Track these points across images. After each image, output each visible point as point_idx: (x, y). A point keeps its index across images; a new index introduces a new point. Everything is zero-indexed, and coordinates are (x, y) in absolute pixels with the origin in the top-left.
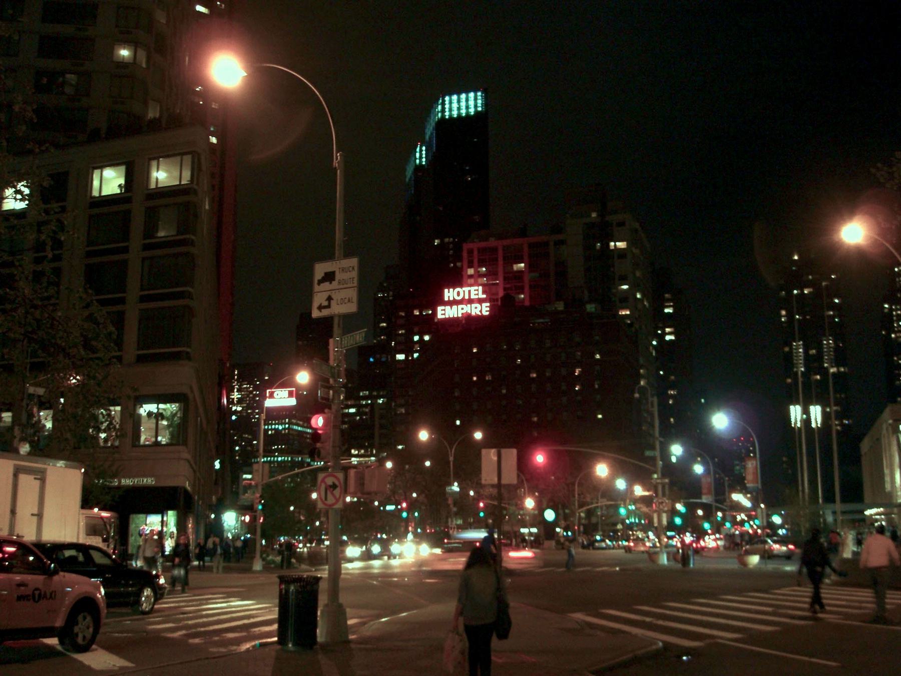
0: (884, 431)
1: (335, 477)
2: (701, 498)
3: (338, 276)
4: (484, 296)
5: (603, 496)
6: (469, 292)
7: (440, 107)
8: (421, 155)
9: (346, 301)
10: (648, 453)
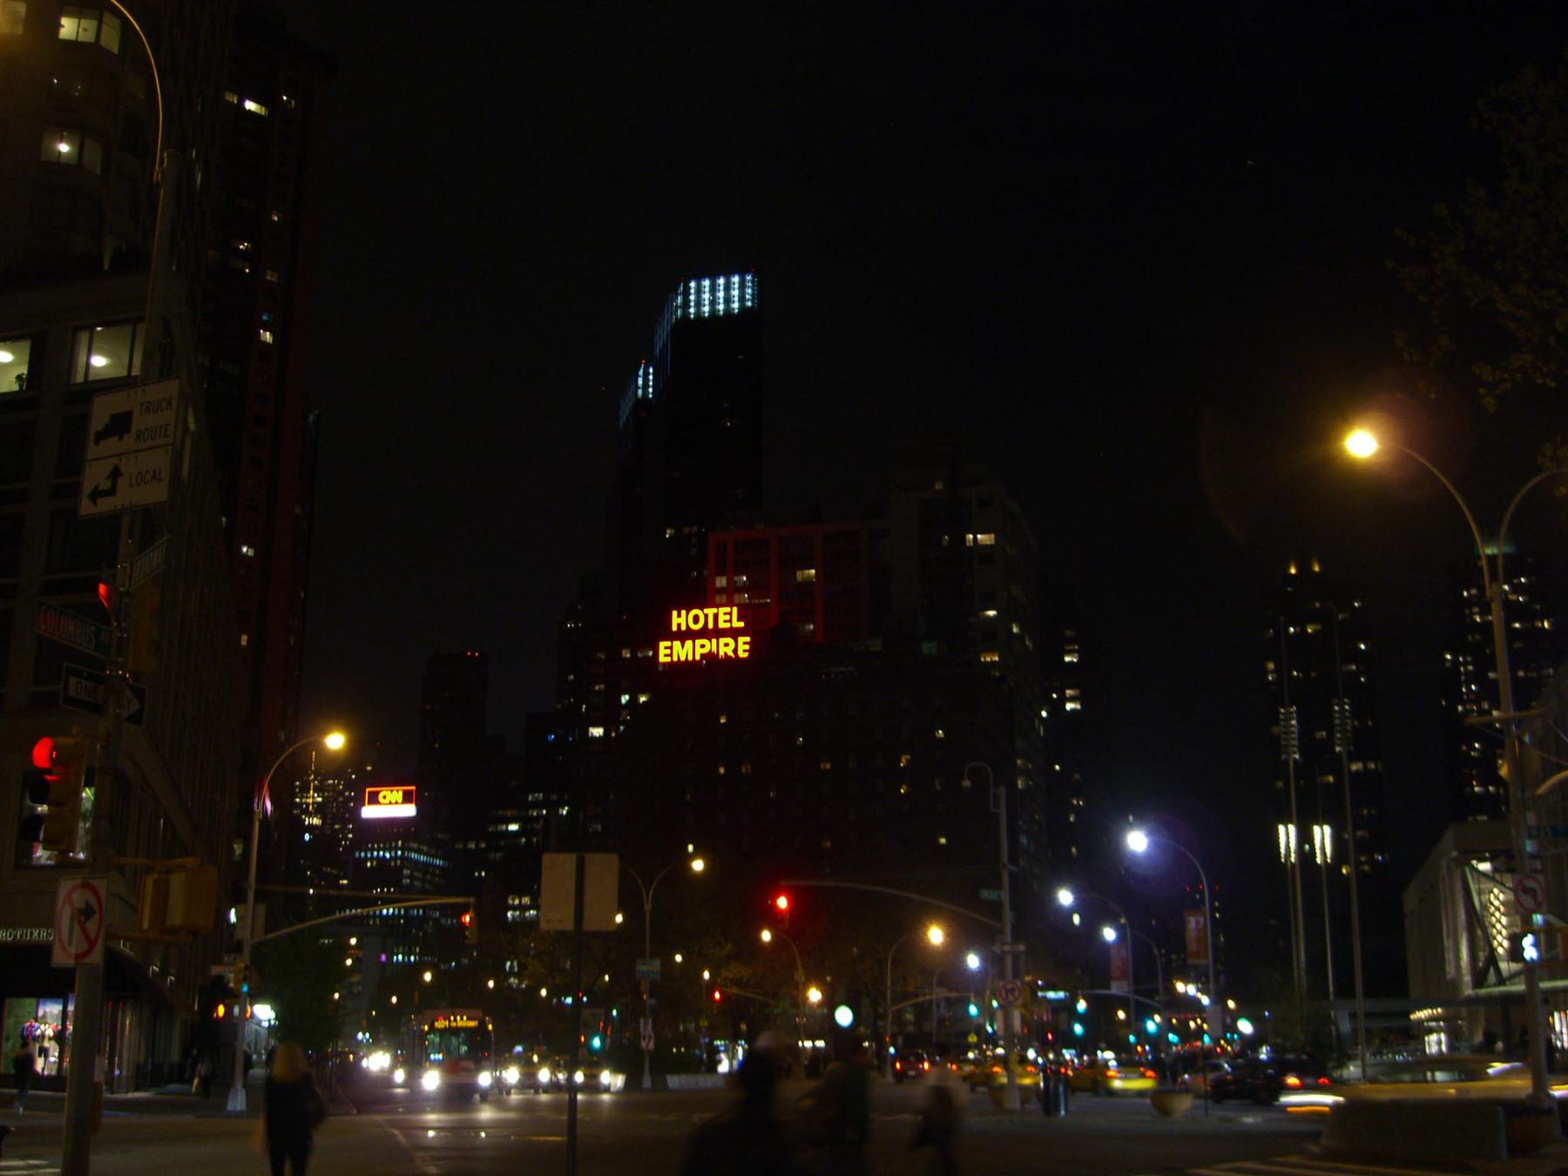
0: (1444, 872)
1: (93, 889)
2: (1108, 987)
3: (137, 423)
4: (742, 624)
5: (941, 984)
6: (716, 616)
7: (680, 300)
8: (645, 382)
9: (149, 476)
10: (986, 894)
